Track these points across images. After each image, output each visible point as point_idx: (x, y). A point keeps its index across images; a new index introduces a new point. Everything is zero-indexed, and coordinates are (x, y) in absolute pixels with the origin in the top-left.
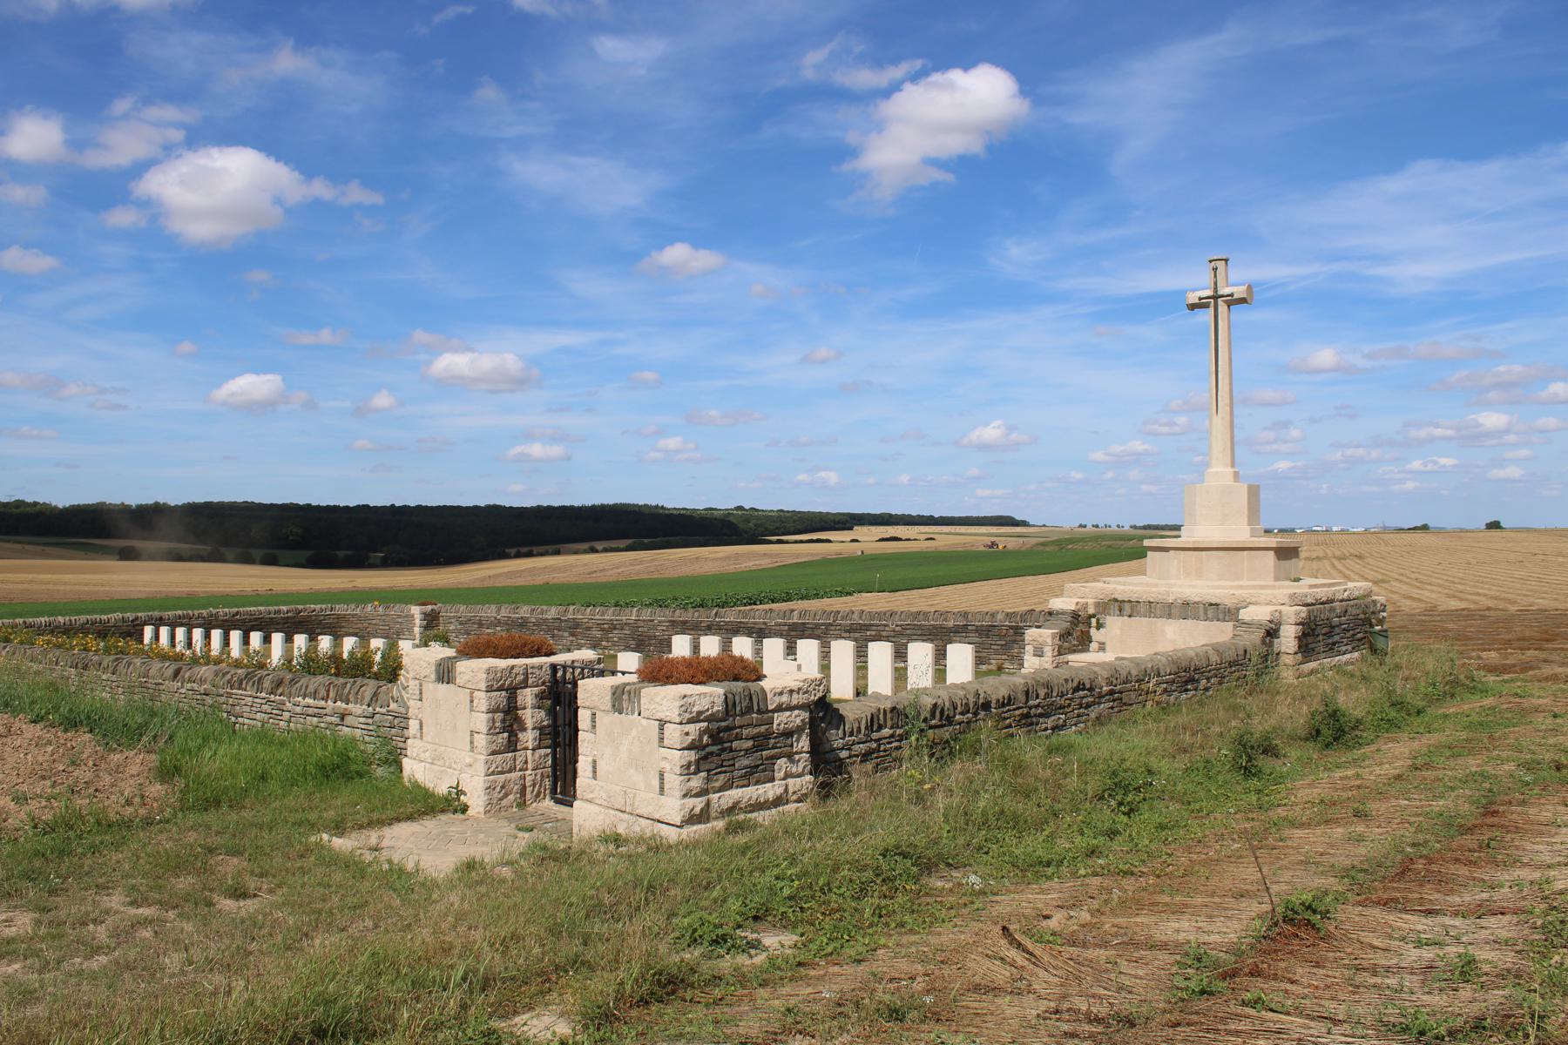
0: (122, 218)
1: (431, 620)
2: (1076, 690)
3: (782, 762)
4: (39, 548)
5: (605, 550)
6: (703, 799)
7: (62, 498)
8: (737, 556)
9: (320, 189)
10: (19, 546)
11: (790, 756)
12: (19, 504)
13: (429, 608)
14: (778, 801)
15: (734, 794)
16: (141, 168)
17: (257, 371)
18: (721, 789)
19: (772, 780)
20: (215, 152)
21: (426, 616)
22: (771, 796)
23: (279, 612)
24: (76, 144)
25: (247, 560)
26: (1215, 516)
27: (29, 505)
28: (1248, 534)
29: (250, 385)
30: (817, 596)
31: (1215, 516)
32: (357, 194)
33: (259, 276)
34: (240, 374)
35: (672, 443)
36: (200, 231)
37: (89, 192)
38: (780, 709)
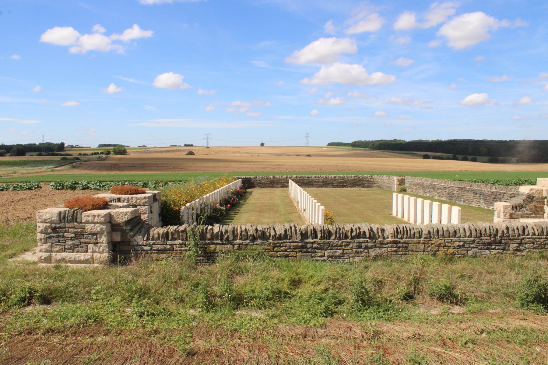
0: (434, 44)
1: (401, 182)
2: (358, 236)
3: (91, 246)
4: (399, 155)
6: (48, 254)
9: (505, 23)
10: (393, 154)
11: (96, 243)
12: (395, 140)
13: (401, 178)
14: (86, 262)
15: (64, 255)
16: (440, 25)
17: (479, 92)
18: (58, 251)
19: (87, 252)
20: (465, 15)
21: (399, 180)
22: (82, 258)
23: (351, 177)
24: (420, 20)
27: (398, 141)
29: (474, 98)
32: (518, 23)
36: (459, 45)
37: (423, 35)
38: (87, 222)
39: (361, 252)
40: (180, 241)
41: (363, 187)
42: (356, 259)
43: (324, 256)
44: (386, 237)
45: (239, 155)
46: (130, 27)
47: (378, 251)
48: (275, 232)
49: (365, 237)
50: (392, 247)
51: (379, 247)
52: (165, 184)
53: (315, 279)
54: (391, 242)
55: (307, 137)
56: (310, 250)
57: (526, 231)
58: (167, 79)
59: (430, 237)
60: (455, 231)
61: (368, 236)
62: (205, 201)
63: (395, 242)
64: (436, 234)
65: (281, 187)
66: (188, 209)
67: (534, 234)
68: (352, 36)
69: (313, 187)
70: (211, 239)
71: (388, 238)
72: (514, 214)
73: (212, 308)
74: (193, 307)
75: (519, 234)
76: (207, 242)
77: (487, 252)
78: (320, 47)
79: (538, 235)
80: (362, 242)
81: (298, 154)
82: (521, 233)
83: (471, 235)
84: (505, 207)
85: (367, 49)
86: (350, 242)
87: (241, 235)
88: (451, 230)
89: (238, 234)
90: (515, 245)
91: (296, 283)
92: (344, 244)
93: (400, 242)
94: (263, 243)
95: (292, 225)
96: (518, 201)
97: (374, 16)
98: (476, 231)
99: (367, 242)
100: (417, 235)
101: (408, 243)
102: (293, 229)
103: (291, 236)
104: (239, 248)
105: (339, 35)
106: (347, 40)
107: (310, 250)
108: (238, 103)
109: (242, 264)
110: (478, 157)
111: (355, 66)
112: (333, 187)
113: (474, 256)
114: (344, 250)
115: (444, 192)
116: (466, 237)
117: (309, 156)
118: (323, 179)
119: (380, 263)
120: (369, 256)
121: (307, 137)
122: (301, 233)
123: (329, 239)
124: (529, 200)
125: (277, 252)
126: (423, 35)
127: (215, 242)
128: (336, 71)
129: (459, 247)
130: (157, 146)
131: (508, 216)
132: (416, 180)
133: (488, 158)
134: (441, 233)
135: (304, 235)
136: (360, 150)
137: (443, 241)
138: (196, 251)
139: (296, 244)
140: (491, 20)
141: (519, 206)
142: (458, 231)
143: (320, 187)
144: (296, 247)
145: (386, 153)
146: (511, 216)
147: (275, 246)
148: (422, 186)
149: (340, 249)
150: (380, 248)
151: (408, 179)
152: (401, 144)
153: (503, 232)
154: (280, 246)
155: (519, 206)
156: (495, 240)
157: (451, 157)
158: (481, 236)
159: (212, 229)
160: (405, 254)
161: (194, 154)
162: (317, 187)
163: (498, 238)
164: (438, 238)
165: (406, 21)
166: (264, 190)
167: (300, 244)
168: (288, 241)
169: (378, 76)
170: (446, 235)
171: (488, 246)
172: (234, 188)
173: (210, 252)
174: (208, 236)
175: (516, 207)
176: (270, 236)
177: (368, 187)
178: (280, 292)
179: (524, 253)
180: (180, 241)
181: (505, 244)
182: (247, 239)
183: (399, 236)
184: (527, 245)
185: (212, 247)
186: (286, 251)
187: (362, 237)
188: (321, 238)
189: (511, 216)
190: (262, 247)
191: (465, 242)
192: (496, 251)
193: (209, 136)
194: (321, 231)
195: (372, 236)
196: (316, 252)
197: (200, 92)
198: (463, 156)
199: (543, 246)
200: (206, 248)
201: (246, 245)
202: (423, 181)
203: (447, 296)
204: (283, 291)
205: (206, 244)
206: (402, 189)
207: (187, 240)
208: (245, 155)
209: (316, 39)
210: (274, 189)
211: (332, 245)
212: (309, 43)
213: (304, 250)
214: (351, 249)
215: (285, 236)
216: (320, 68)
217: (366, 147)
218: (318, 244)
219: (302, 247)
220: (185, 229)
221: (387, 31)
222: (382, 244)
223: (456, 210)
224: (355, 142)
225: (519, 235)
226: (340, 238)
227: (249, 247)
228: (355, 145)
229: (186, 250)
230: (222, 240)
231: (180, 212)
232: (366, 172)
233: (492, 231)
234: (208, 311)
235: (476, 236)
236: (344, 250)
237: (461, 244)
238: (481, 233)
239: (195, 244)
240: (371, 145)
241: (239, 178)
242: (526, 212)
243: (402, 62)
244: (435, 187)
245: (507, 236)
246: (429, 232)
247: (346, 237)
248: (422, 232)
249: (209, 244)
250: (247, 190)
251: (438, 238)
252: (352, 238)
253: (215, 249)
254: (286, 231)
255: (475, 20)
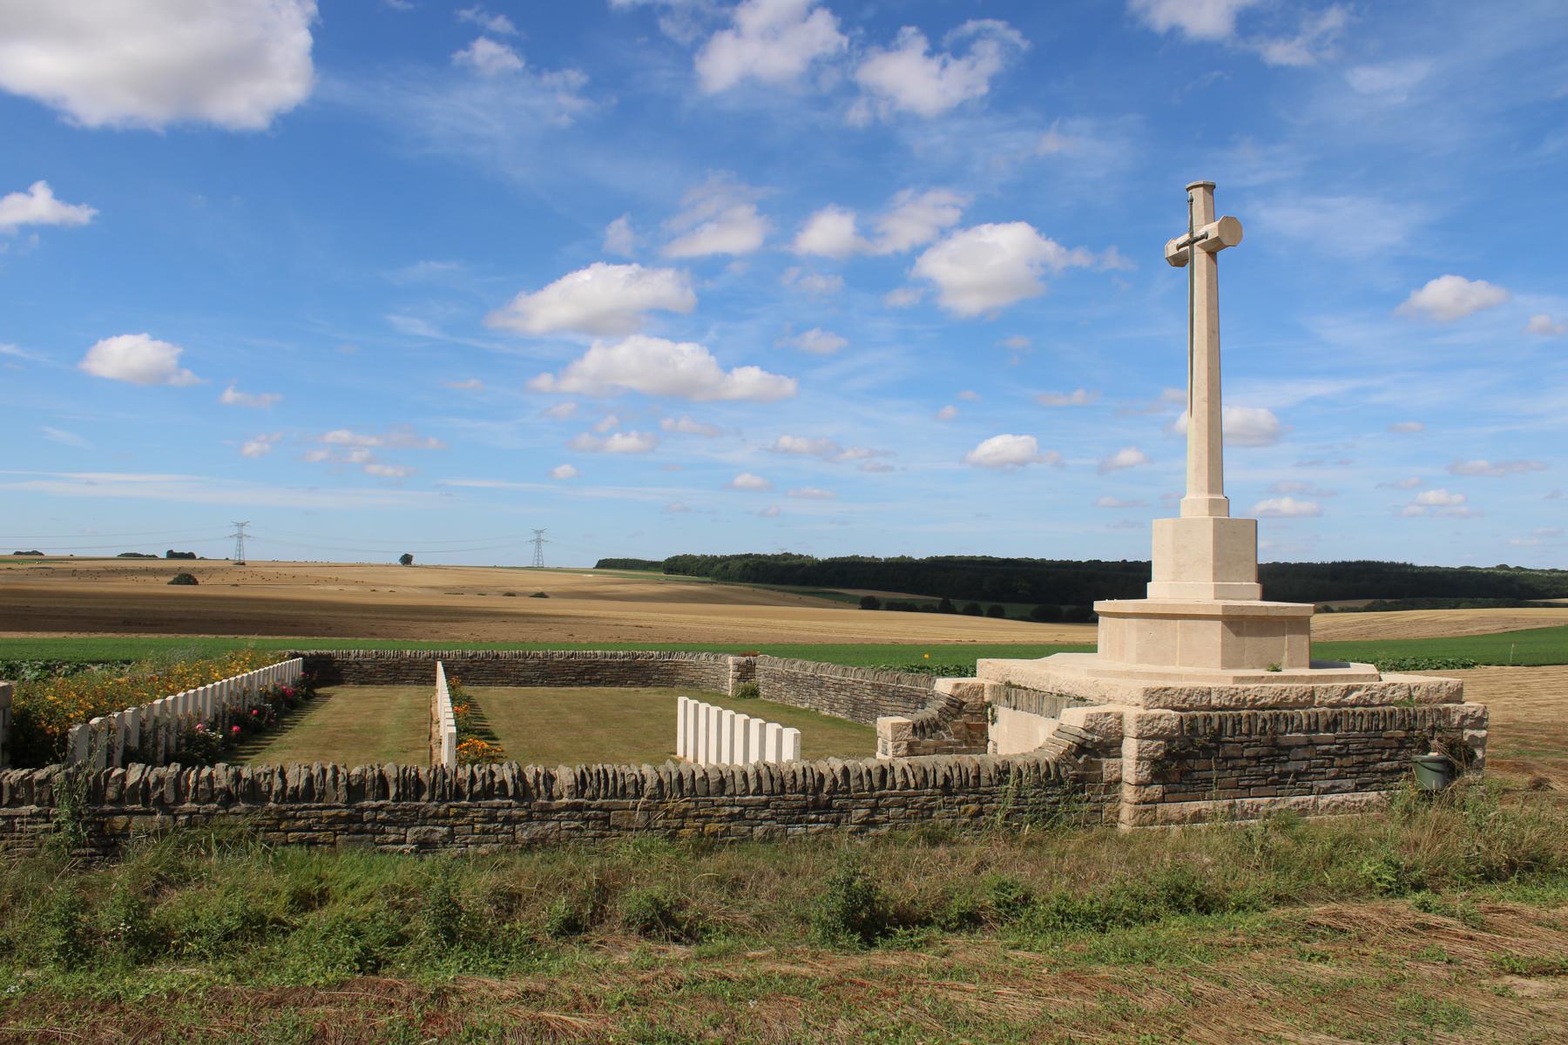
0: (901, 298)
1: (746, 671)
2: (488, 792)
4: (796, 597)
5: (1342, 610)
7: (823, 551)
8: (1482, 620)
9: (1080, 258)
10: (781, 594)
12: (787, 556)
16: (918, 250)
17: (1016, 432)
20: (985, 229)
21: (739, 666)
23: (615, 656)
24: (866, 232)
25: (973, 611)
26: (1184, 578)
28: (1211, 594)
30: (1416, 667)
31: (1184, 578)
32: (1113, 260)
33: (1018, 341)
34: (990, 437)
35: (1432, 496)
36: (971, 304)
37: (874, 274)
39: (496, 832)
40: (34, 808)
41: (645, 684)
42: (483, 850)
43: (404, 842)
44: (556, 793)
45: (336, 588)
46: (24, 188)
47: (537, 829)
48: (284, 782)
49: (506, 796)
50: (570, 818)
51: (538, 819)
52: (76, 670)
53: (359, 891)
54: (568, 807)
55: (539, 541)
56: (369, 826)
57: (889, 777)
58: (126, 353)
59: (662, 795)
60: (722, 781)
61: (511, 793)
62: (157, 713)
63: (577, 807)
64: (676, 786)
65: (418, 682)
66: (94, 732)
67: (906, 785)
68: (680, 264)
69: (508, 684)
70: (119, 800)
71: (561, 797)
72: (918, 744)
73: (82, 961)
74: (33, 964)
75: (872, 785)
76: (107, 808)
77: (799, 830)
78: (592, 287)
79: (916, 788)
80: (498, 808)
81: (512, 589)
82: (876, 783)
83: (759, 790)
84: (897, 729)
85: (721, 303)
86: (468, 807)
87: (196, 788)
88: (714, 777)
89: (188, 787)
90: (862, 812)
91: (305, 901)
92: (453, 811)
93: (588, 808)
94: (251, 810)
95: (329, 767)
96: (930, 712)
97: (743, 212)
98: (772, 779)
99: (510, 806)
100: (631, 790)
101: (609, 810)
102: (329, 774)
103: (323, 793)
104: (190, 824)
105: (646, 258)
106: (669, 274)
107: (369, 826)
108: (344, 435)
109: (189, 862)
110: (1006, 606)
111: (685, 348)
112: (563, 685)
113: (768, 838)
114: (452, 826)
115: (843, 695)
116: (747, 793)
117: (542, 595)
118: (536, 661)
119: (538, 856)
120: (515, 842)
121: (539, 541)
122: (348, 786)
123: (417, 800)
124: (953, 710)
125: (287, 832)
126: (874, 274)
127: (129, 807)
128: (634, 358)
129: (732, 817)
130: (76, 555)
131: (903, 750)
132: (780, 666)
133: (1032, 607)
134: (687, 785)
135: (356, 791)
136: (689, 583)
137: (692, 805)
138: (75, 832)
139: (334, 812)
140: (1049, 247)
141: (929, 725)
142: (729, 781)
143: (528, 682)
144: (336, 819)
145: (760, 590)
146: (912, 750)
147: (282, 816)
148: (793, 680)
149: (443, 825)
150: (542, 821)
151: (764, 664)
152: (802, 566)
153: (835, 780)
154: (294, 817)
155: (929, 725)
156: (815, 801)
157: (937, 605)
158: (783, 791)
159: (123, 777)
160: (602, 836)
161: (196, 583)
162: (520, 684)
163: (824, 796)
164: (682, 796)
165: (829, 232)
166: (369, 691)
167: (345, 812)
168: (314, 805)
169: (748, 378)
170: (700, 788)
171: (798, 815)
172: (270, 684)
173: (113, 835)
174: (111, 793)
175: (922, 728)
176: (270, 791)
177: (659, 683)
178: (262, 920)
179: (885, 830)
180: (34, 808)
181: (841, 809)
182: (211, 800)
183: (588, 792)
184: (892, 811)
185: (120, 821)
186: (309, 829)
187: (499, 796)
188: (398, 798)
189: (912, 750)
190: (248, 820)
191: (746, 807)
192: (820, 827)
193: (246, 531)
194: (397, 780)
195: (523, 791)
196: (383, 832)
197: (230, 396)
198: (968, 603)
199: (927, 813)
200: (103, 824)
201: (209, 815)
202: (796, 667)
203: (662, 922)
204: (270, 917)
205: (104, 814)
206: (746, 689)
207: (52, 803)
208: (354, 588)
209: (586, 264)
210: (397, 688)
211: (424, 814)
212: (560, 275)
213: (356, 826)
214: (472, 823)
215: (308, 792)
216: (588, 348)
217: (706, 574)
218: (389, 812)
219: (349, 819)
220: (49, 776)
221: (774, 260)
222: (546, 813)
223: (790, 734)
224: (676, 559)
225: (872, 789)
226: (443, 799)
227: (215, 821)
228: (677, 566)
229: (46, 831)
230: (146, 802)
231: (66, 742)
232: (653, 647)
233: (809, 781)
234: (70, 968)
235: (772, 793)
236: (452, 826)
237: (737, 810)
238: (783, 785)
239: (73, 813)
240: (718, 567)
241: (296, 656)
242: (947, 739)
243: (816, 341)
244: (821, 684)
245: (844, 792)
246: (660, 782)
247: (459, 795)
248: (644, 781)
249: (112, 813)
250: (318, 691)
251: (682, 796)
252: (475, 797)
253: (126, 827)
254: (310, 780)
255: (1008, 245)
